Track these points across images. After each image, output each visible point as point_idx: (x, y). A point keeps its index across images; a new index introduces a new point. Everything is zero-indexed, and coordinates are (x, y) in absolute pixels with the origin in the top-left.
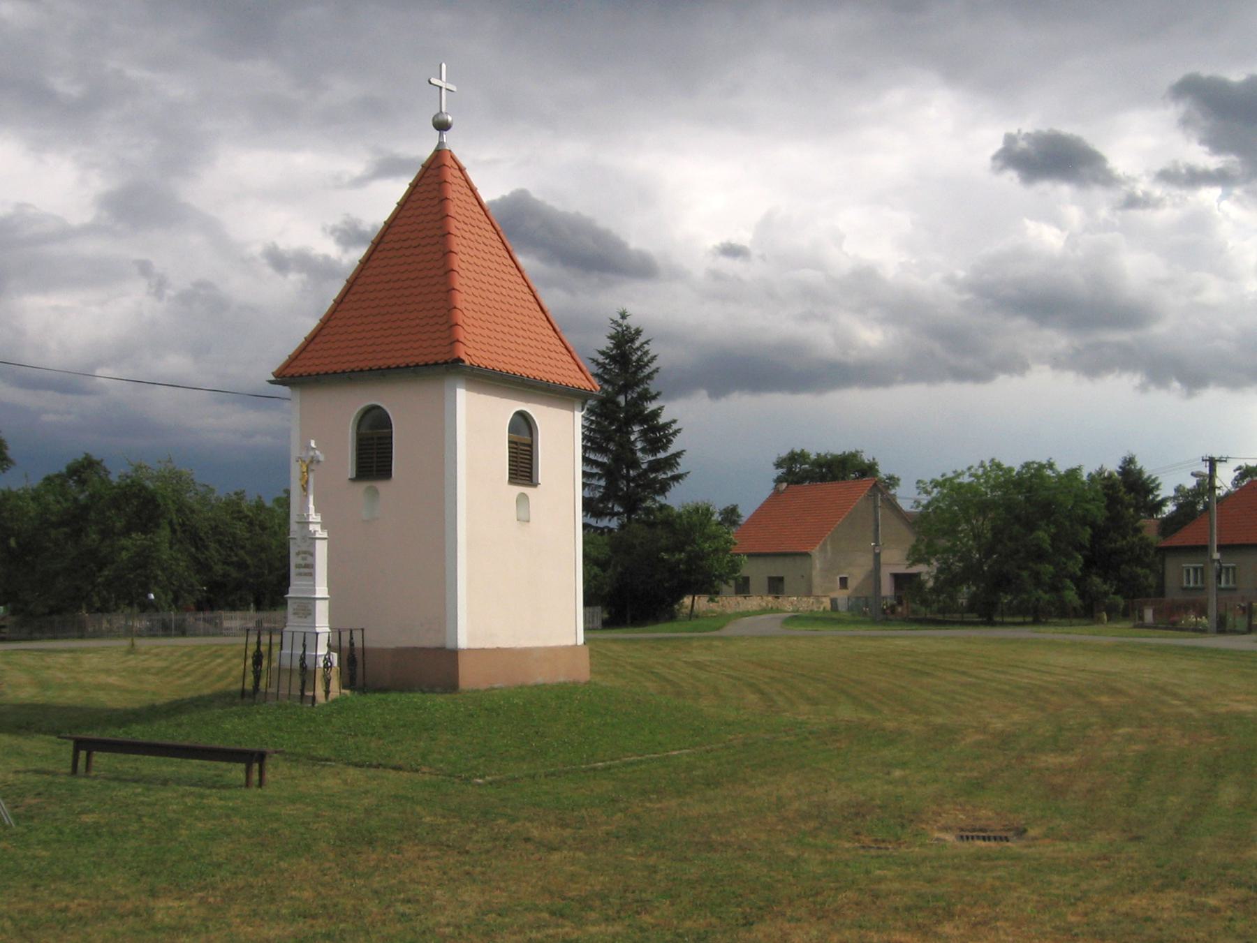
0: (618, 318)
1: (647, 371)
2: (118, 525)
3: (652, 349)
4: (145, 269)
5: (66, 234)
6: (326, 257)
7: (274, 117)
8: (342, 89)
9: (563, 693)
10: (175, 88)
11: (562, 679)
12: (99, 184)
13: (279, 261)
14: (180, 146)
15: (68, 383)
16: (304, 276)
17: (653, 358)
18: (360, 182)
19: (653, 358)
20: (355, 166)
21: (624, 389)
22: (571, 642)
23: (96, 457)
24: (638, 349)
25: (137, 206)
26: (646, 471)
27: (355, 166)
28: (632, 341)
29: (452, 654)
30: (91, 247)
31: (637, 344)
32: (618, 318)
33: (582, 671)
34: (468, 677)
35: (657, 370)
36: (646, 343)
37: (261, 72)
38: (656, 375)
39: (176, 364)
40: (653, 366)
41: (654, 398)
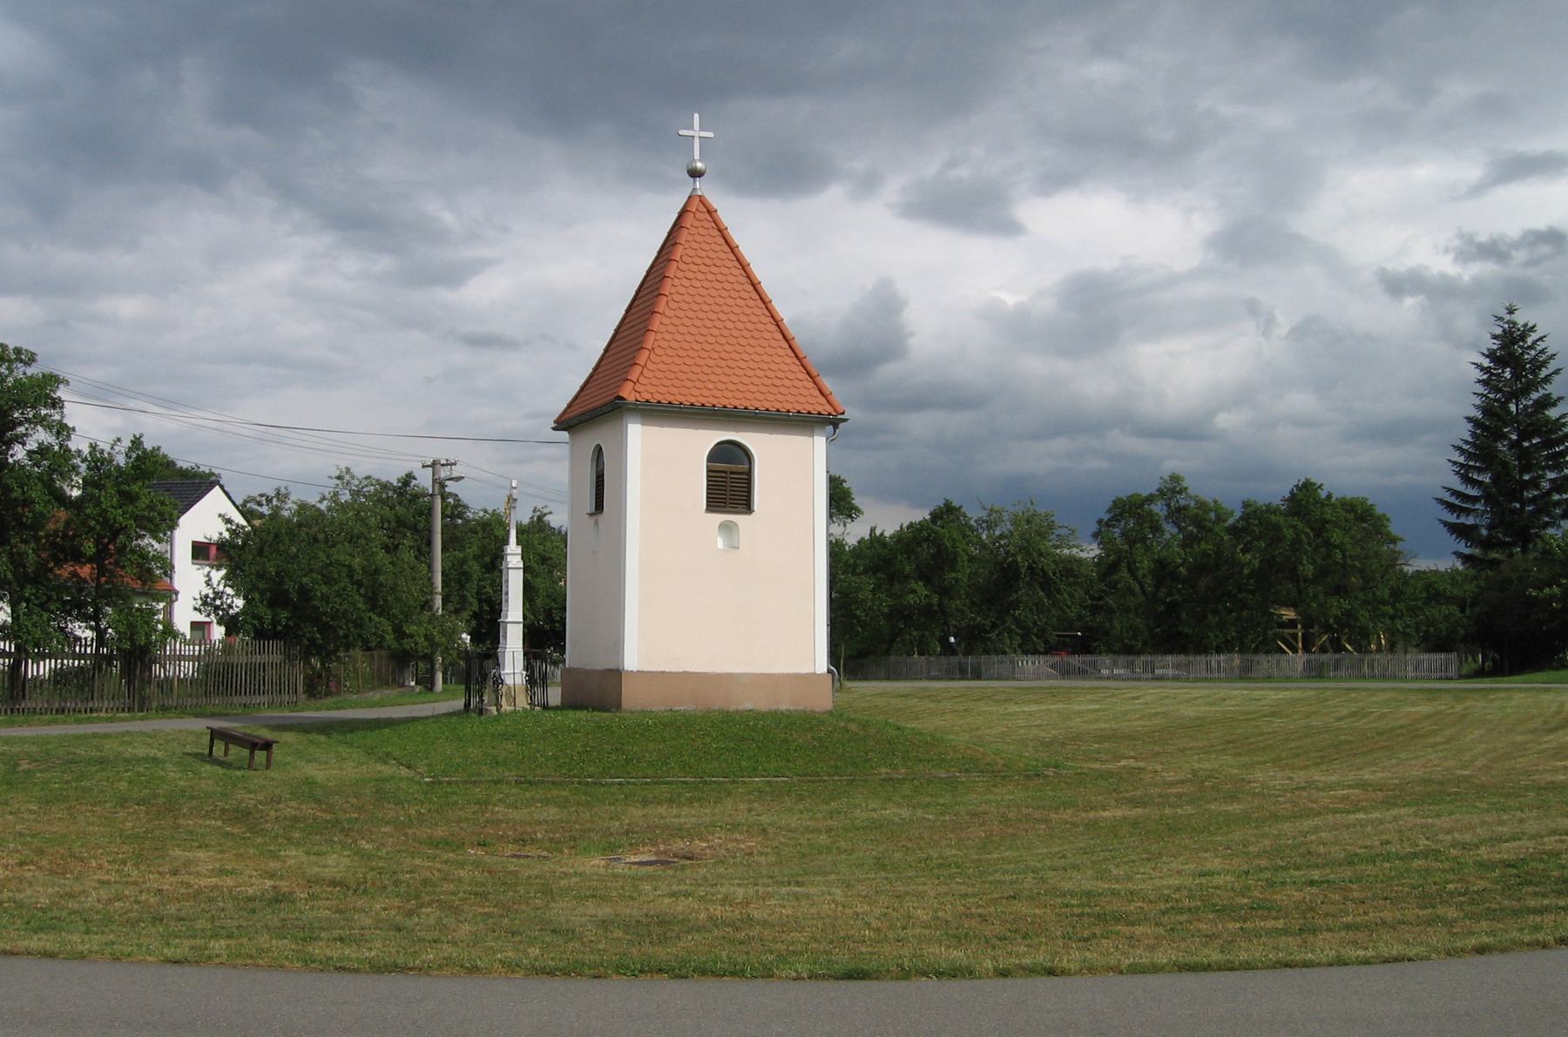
0: (1503, 313)
1: (1544, 373)
2: (908, 568)
3: (1550, 345)
4: (1252, 308)
5: (1173, 281)
6: (1443, 276)
7: (1382, 131)
8: (1457, 90)
9: (802, 722)
10: (1277, 118)
11: (783, 707)
12: (1205, 224)
13: (1397, 285)
14: (1283, 177)
15: (1187, 432)
16: (1421, 298)
17: (1552, 357)
18: (1477, 190)
19: (1552, 357)
20: (1471, 170)
21: (1515, 395)
22: (805, 669)
23: (956, 504)
24: (1530, 348)
25: (1245, 244)
26: (1549, 493)
27: (1471, 170)
28: (1523, 337)
29: (616, 674)
30: (1200, 290)
31: (1529, 341)
32: (1503, 313)
33: (823, 700)
34: (632, 697)
35: (1557, 372)
36: (1541, 339)
37: (1367, 90)
38: (1556, 378)
39: (1300, 401)
40: (1552, 366)
41: (1554, 404)
